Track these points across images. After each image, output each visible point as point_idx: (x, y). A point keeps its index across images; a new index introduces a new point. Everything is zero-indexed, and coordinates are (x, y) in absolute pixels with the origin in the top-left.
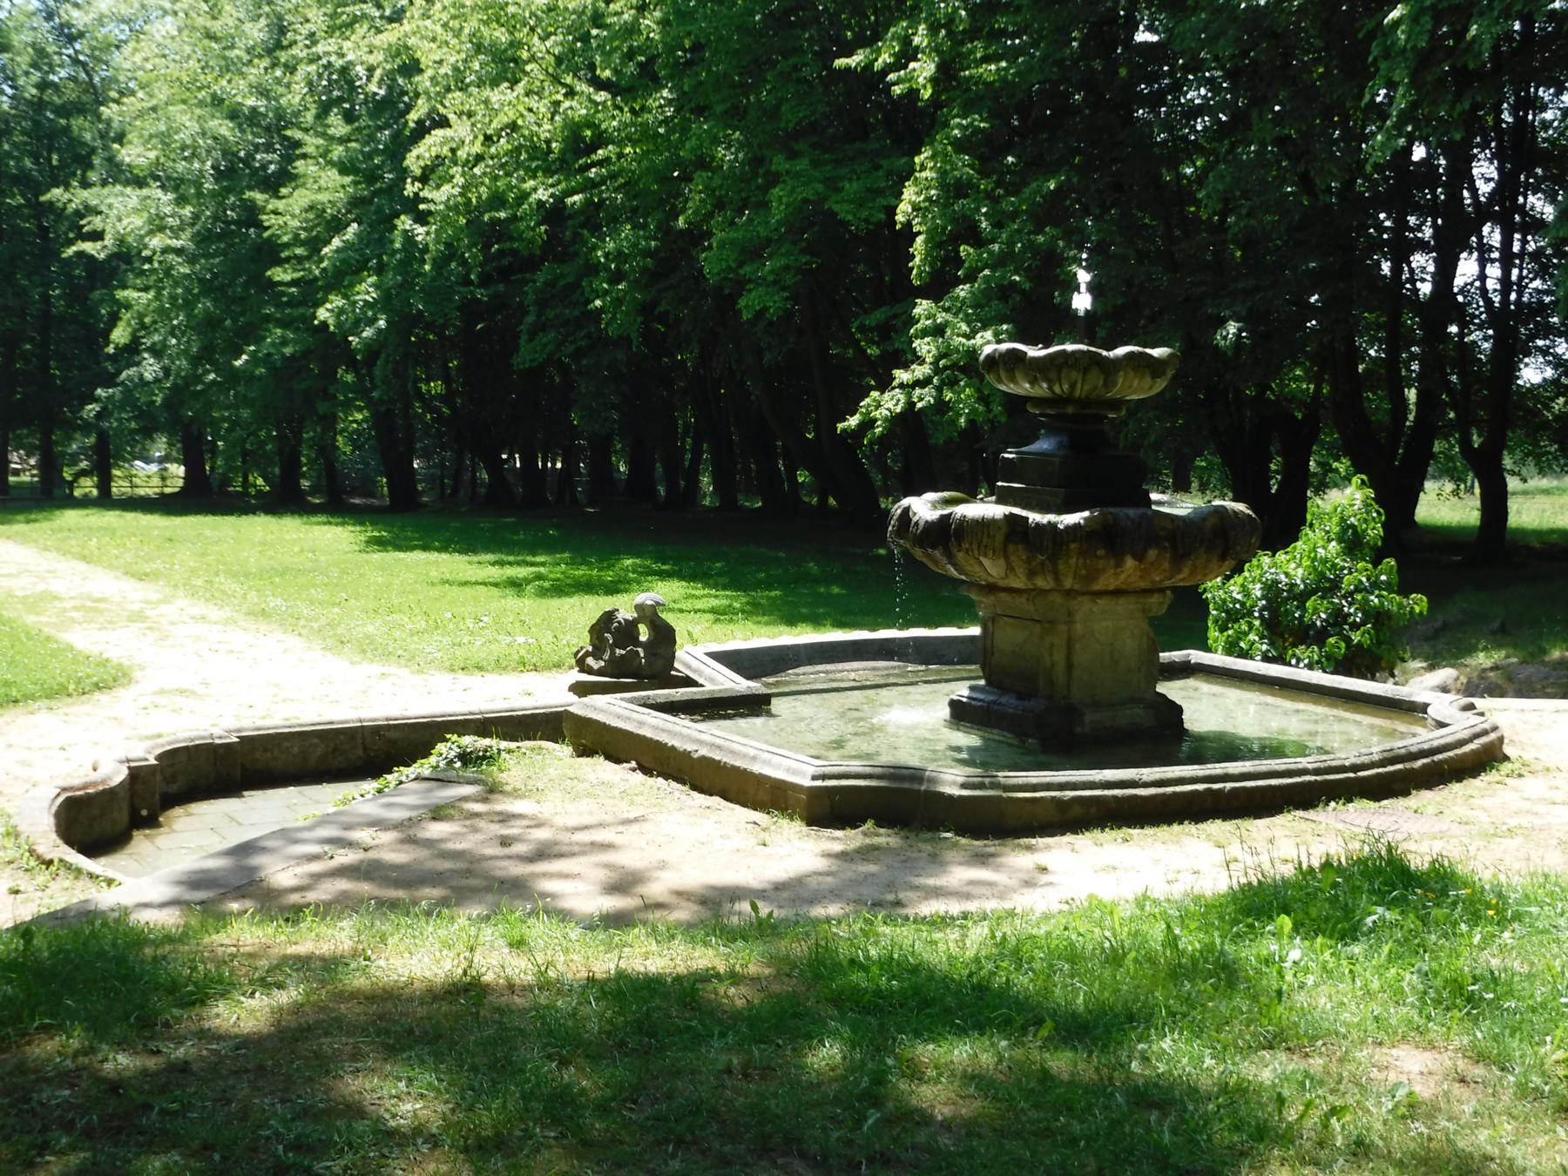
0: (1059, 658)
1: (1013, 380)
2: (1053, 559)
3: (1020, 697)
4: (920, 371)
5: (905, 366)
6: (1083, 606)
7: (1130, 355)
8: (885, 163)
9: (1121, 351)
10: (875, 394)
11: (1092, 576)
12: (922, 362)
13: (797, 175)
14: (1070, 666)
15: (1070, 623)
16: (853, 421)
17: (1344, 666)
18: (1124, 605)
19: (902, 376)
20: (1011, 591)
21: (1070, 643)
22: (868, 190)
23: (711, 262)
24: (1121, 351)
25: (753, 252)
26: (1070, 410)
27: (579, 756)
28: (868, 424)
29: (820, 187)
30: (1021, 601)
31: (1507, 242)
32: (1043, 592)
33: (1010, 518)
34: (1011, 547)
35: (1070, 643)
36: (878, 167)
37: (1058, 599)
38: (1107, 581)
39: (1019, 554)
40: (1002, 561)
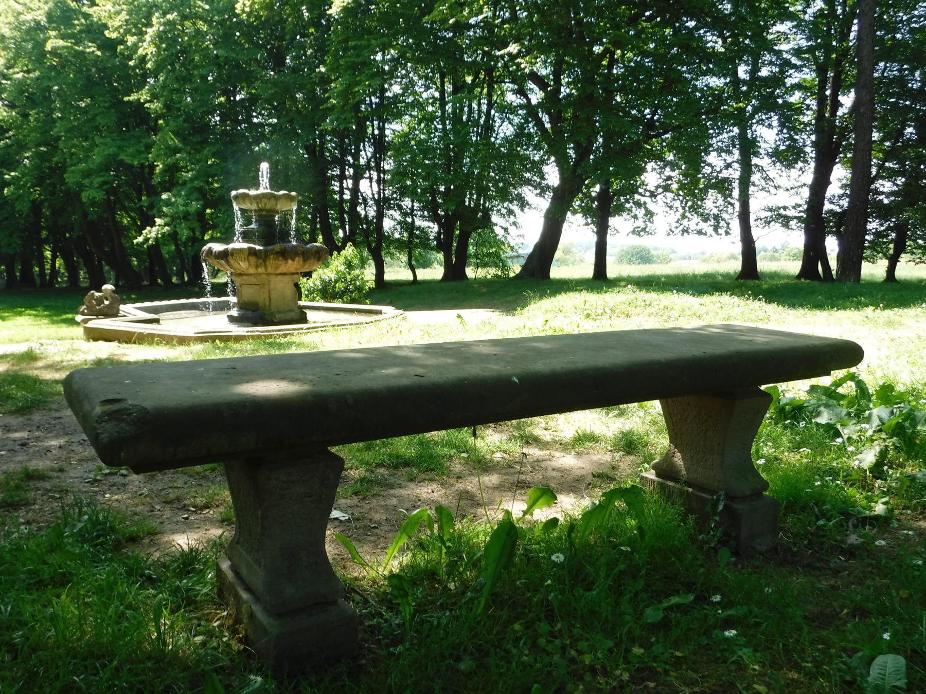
0: (267, 296)
1: (244, 203)
2: (265, 261)
3: (253, 311)
6: (274, 279)
7: (284, 195)
8: (144, 141)
9: (282, 192)
10: (148, 228)
11: (277, 268)
13: (105, 144)
15: (269, 284)
16: (140, 239)
17: (353, 301)
18: (286, 279)
20: (251, 275)
21: (269, 291)
22: (137, 151)
23: (70, 178)
24: (282, 192)
25: (88, 174)
26: (264, 213)
27: (88, 340)
28: (147, 240)
29: (115, 149)
30: (252, 278)
31: (379, 176)
32: (260, 274)
33: (250, 248)
34: (250, 258)
35: (269, 291)
36: (140, 142)
37: (264, 276)
38: (283, 269)
39: (253, 259)
40: (247, 263)
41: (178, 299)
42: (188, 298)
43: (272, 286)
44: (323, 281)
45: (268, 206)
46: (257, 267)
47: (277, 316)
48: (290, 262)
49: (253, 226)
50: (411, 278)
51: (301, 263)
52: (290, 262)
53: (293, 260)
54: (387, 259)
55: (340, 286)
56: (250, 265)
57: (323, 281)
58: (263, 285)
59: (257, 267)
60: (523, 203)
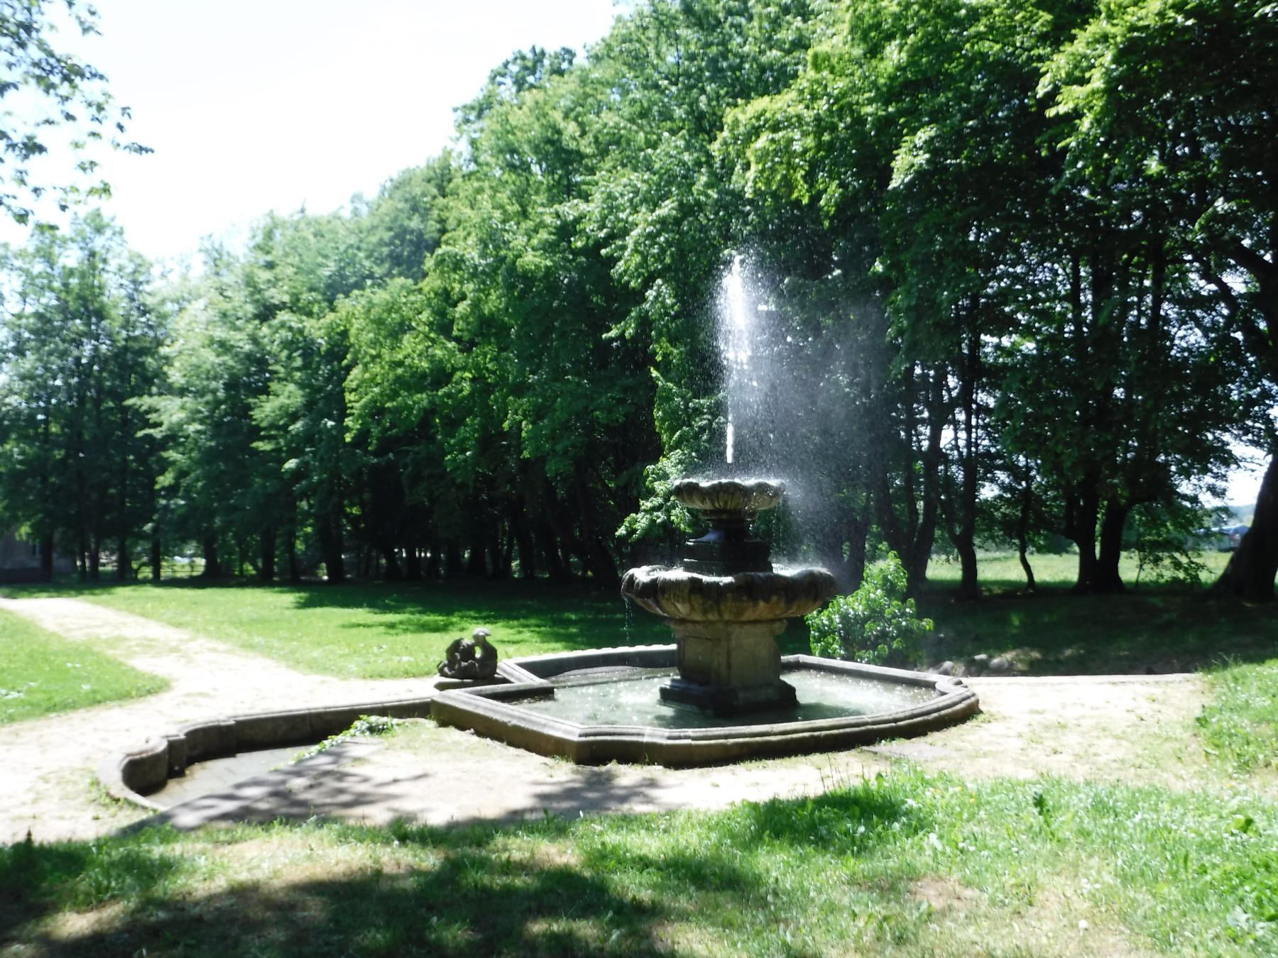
4: (657, 501)
5: (647, 499)
6: (736, 630)
11: (740, 612)
12: (657, 496)
14: (729, 666)
15: (729, 640)
16: (622, 531)
18: (759, 629)
19: (646, 504)
26: (724, 517)
32: (712, 623)
33: (692, 580)
34: (693, 597)
35: (729, 654)
37: (721, 626)
38: (749, 615)
39: (697, 601)
40: (688, 605)
41: (599, 647)
42: (614, 646)
43: (733, 643)
44: (845, 617)
45: (730, 505)
46: (705, 612)
47: (741, 695)
48: (762, 604)
49: (710, 537)
50: (1024, 577)
51: (782, 605)
52: (762, 604)
53: (767, 600)
54: (980, 555)
55: (872, 629)
56: (693, 608)
57: (845, 617)
58: (718, 640)
59: (705, 612)
60: (1228, 459)
